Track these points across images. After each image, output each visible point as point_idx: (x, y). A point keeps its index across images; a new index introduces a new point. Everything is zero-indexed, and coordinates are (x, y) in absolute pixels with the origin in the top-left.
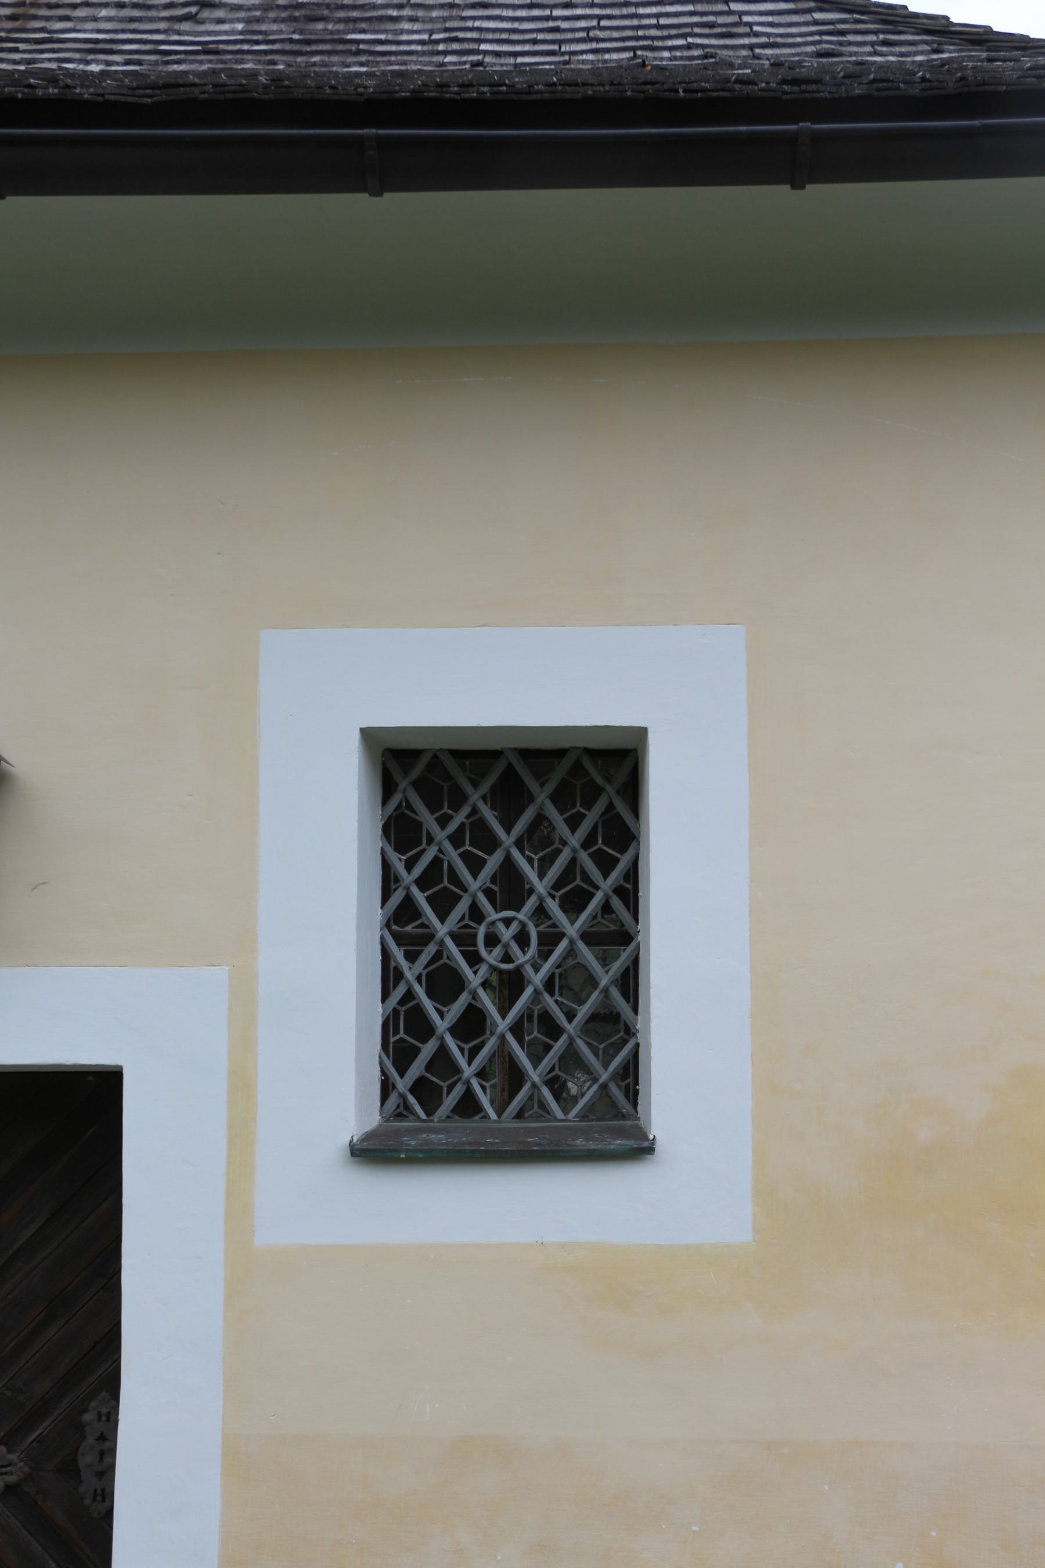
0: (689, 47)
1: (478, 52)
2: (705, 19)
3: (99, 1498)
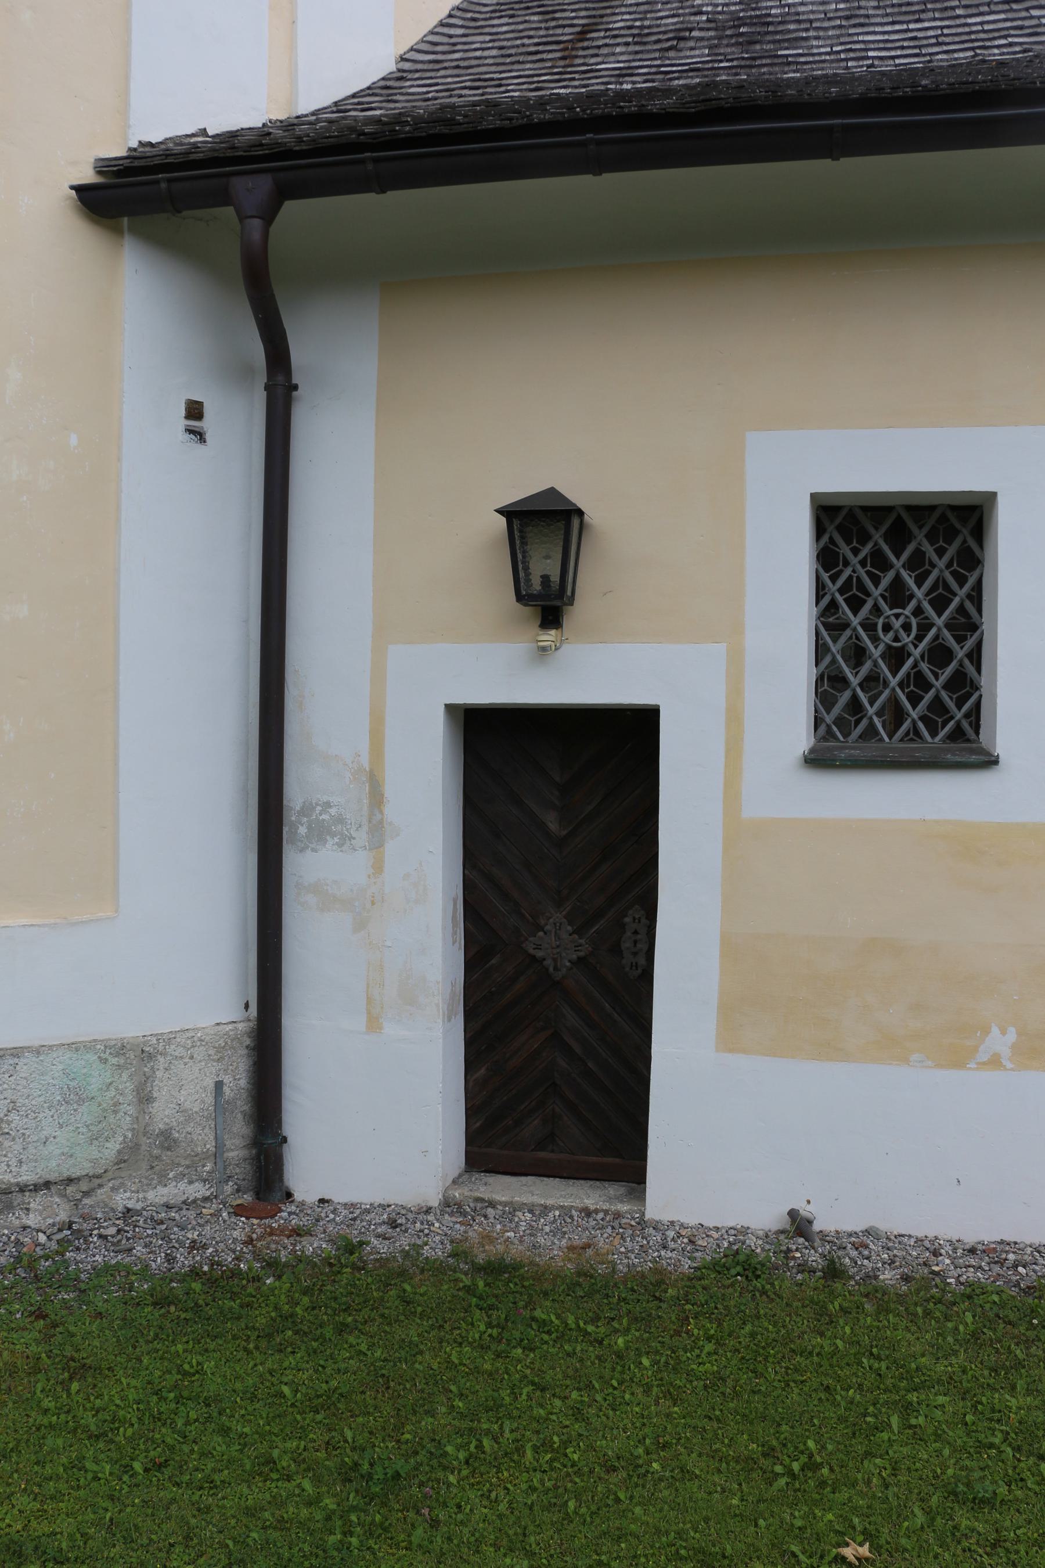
0: (1011, 45)
1: (868, 58)
2: (1015, 24)
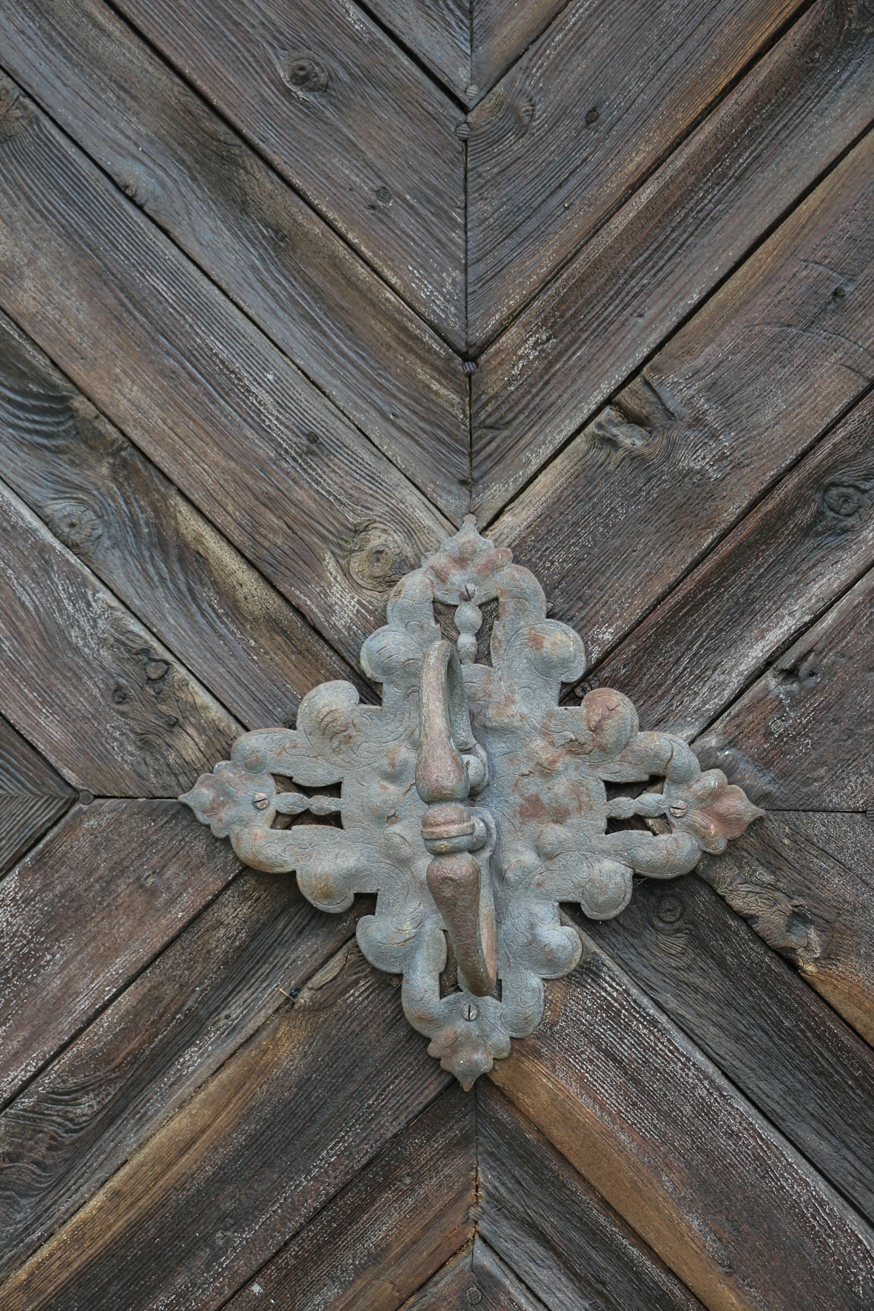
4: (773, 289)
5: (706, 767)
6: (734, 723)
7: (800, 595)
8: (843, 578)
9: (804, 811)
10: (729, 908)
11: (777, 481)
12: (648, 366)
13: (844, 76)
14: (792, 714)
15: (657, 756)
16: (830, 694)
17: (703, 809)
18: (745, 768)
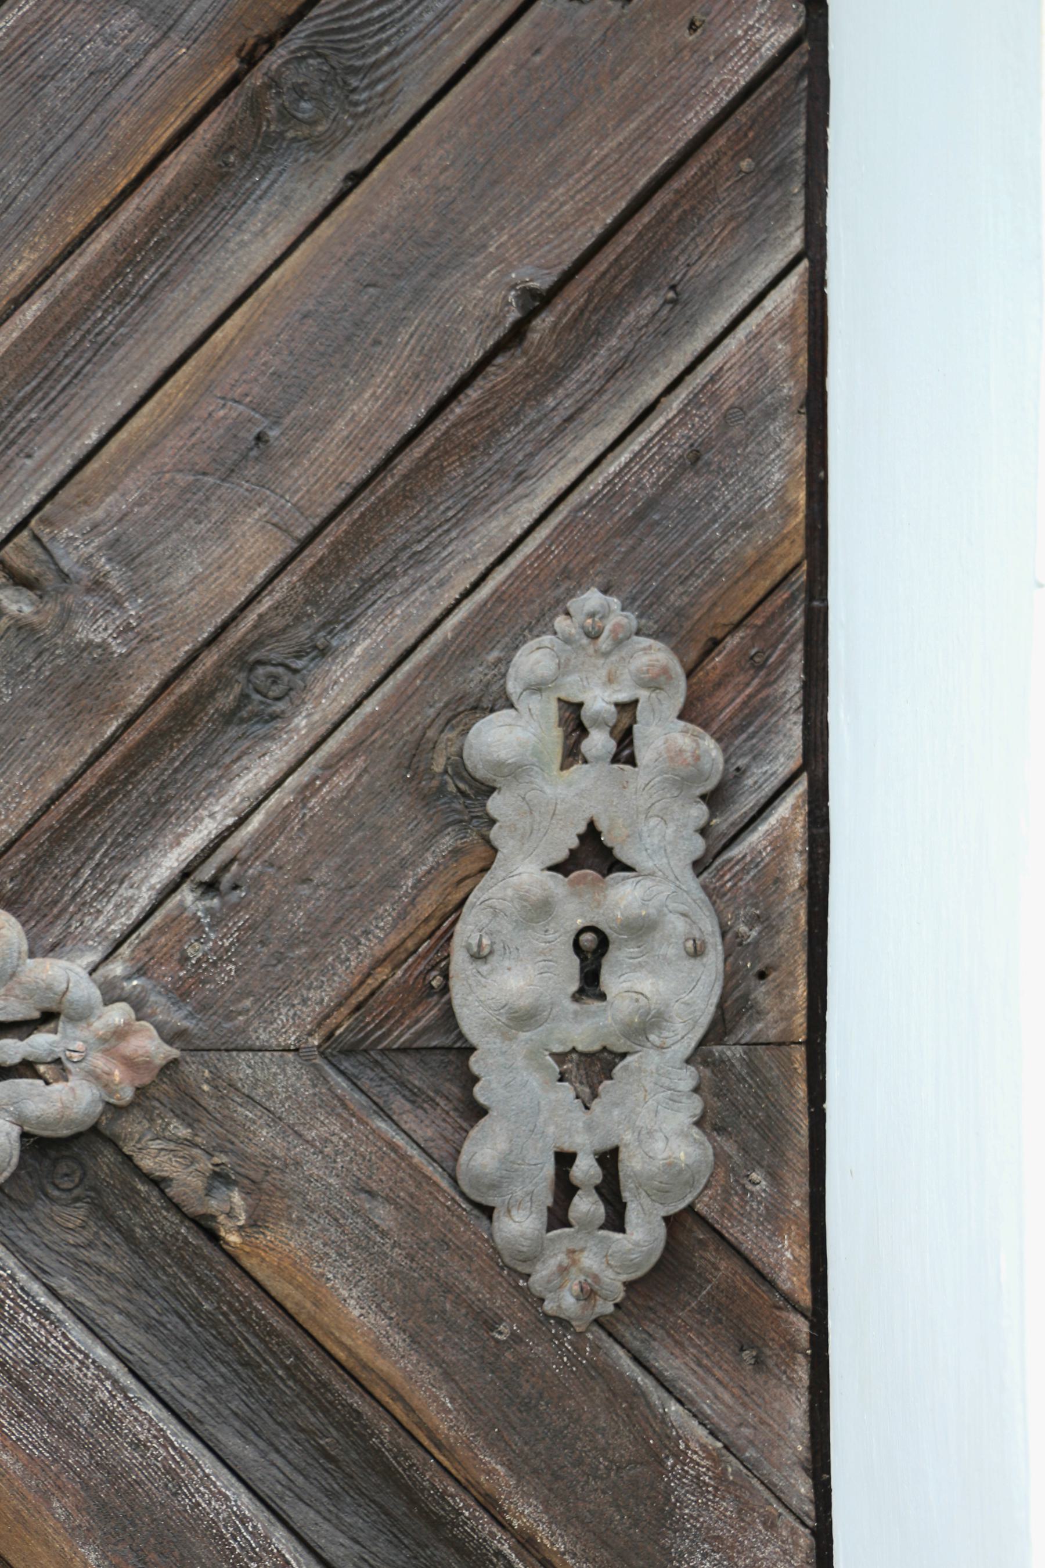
3: (586, 1205)
4: (185, 430)
5: (108, 1001)
6: (144, 946)
7: (222, 793)
8: (272, 772)
9: (227, 1050)
10: (137, 1170)
11: (193, 658)
12: (37, 517)
13: (265, 184)
14: (212, 936)
15: (49, 988)
16: (257, 910)
17: (105, 1052)
18: (158, 1002)
